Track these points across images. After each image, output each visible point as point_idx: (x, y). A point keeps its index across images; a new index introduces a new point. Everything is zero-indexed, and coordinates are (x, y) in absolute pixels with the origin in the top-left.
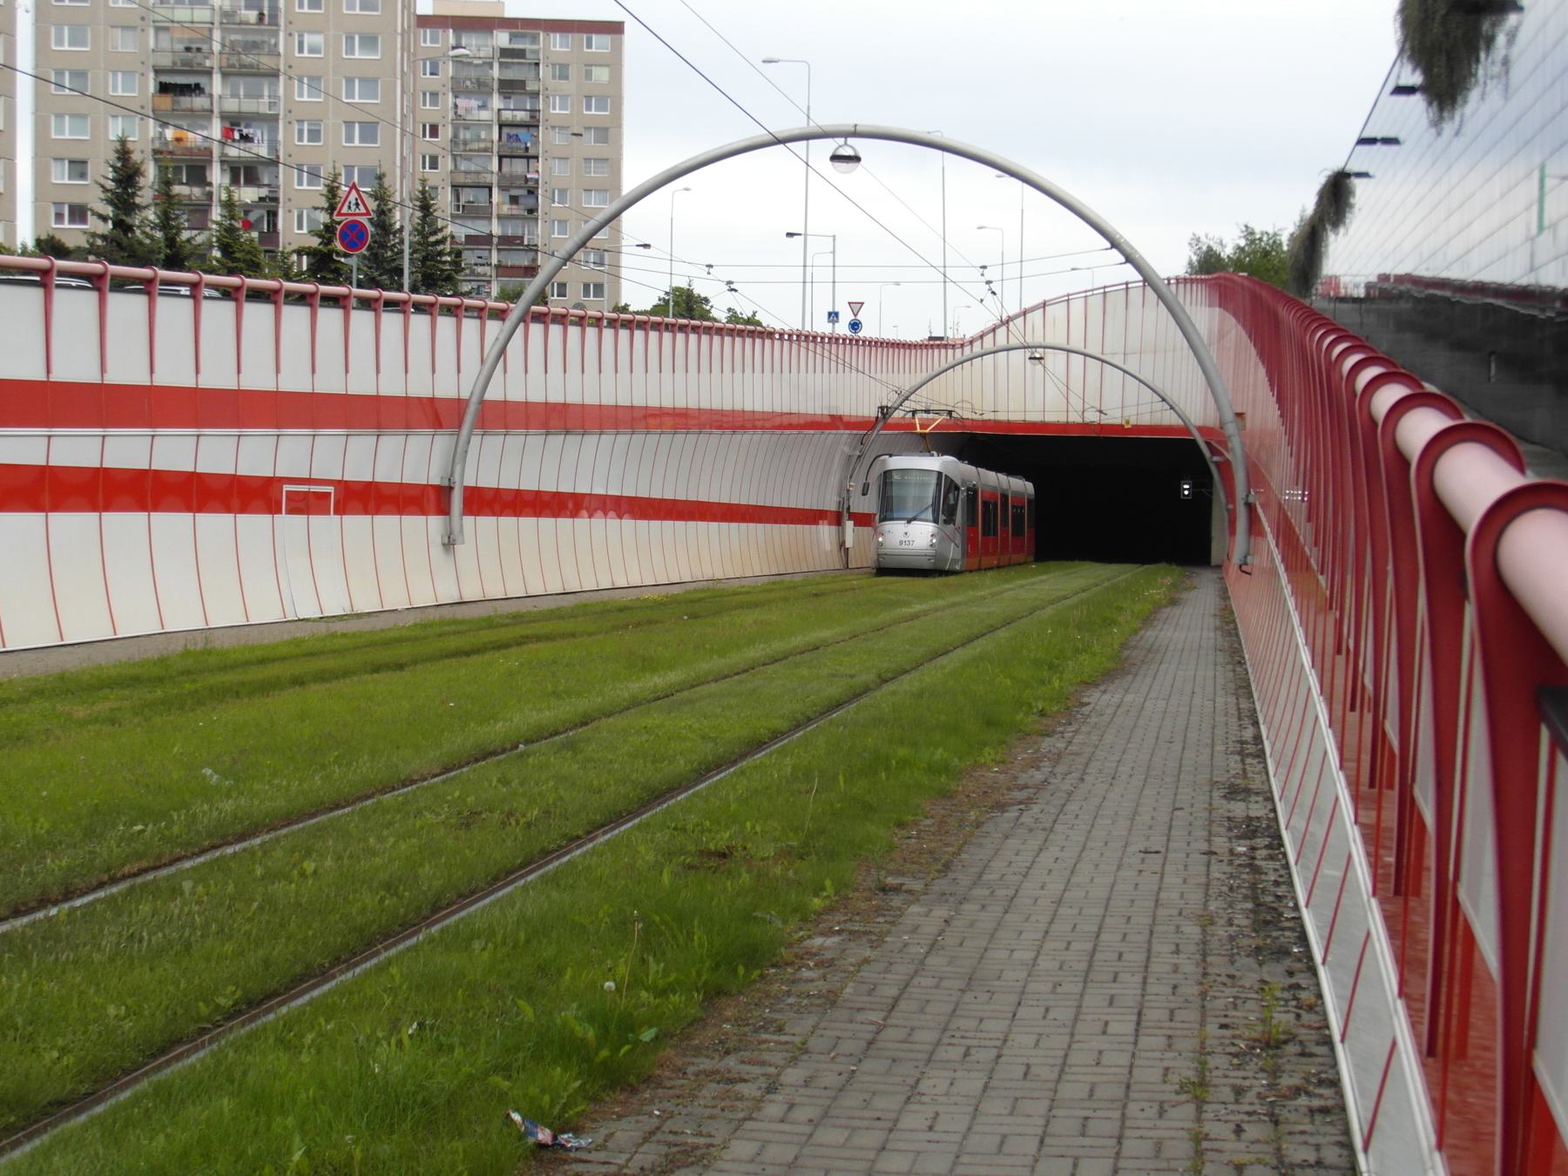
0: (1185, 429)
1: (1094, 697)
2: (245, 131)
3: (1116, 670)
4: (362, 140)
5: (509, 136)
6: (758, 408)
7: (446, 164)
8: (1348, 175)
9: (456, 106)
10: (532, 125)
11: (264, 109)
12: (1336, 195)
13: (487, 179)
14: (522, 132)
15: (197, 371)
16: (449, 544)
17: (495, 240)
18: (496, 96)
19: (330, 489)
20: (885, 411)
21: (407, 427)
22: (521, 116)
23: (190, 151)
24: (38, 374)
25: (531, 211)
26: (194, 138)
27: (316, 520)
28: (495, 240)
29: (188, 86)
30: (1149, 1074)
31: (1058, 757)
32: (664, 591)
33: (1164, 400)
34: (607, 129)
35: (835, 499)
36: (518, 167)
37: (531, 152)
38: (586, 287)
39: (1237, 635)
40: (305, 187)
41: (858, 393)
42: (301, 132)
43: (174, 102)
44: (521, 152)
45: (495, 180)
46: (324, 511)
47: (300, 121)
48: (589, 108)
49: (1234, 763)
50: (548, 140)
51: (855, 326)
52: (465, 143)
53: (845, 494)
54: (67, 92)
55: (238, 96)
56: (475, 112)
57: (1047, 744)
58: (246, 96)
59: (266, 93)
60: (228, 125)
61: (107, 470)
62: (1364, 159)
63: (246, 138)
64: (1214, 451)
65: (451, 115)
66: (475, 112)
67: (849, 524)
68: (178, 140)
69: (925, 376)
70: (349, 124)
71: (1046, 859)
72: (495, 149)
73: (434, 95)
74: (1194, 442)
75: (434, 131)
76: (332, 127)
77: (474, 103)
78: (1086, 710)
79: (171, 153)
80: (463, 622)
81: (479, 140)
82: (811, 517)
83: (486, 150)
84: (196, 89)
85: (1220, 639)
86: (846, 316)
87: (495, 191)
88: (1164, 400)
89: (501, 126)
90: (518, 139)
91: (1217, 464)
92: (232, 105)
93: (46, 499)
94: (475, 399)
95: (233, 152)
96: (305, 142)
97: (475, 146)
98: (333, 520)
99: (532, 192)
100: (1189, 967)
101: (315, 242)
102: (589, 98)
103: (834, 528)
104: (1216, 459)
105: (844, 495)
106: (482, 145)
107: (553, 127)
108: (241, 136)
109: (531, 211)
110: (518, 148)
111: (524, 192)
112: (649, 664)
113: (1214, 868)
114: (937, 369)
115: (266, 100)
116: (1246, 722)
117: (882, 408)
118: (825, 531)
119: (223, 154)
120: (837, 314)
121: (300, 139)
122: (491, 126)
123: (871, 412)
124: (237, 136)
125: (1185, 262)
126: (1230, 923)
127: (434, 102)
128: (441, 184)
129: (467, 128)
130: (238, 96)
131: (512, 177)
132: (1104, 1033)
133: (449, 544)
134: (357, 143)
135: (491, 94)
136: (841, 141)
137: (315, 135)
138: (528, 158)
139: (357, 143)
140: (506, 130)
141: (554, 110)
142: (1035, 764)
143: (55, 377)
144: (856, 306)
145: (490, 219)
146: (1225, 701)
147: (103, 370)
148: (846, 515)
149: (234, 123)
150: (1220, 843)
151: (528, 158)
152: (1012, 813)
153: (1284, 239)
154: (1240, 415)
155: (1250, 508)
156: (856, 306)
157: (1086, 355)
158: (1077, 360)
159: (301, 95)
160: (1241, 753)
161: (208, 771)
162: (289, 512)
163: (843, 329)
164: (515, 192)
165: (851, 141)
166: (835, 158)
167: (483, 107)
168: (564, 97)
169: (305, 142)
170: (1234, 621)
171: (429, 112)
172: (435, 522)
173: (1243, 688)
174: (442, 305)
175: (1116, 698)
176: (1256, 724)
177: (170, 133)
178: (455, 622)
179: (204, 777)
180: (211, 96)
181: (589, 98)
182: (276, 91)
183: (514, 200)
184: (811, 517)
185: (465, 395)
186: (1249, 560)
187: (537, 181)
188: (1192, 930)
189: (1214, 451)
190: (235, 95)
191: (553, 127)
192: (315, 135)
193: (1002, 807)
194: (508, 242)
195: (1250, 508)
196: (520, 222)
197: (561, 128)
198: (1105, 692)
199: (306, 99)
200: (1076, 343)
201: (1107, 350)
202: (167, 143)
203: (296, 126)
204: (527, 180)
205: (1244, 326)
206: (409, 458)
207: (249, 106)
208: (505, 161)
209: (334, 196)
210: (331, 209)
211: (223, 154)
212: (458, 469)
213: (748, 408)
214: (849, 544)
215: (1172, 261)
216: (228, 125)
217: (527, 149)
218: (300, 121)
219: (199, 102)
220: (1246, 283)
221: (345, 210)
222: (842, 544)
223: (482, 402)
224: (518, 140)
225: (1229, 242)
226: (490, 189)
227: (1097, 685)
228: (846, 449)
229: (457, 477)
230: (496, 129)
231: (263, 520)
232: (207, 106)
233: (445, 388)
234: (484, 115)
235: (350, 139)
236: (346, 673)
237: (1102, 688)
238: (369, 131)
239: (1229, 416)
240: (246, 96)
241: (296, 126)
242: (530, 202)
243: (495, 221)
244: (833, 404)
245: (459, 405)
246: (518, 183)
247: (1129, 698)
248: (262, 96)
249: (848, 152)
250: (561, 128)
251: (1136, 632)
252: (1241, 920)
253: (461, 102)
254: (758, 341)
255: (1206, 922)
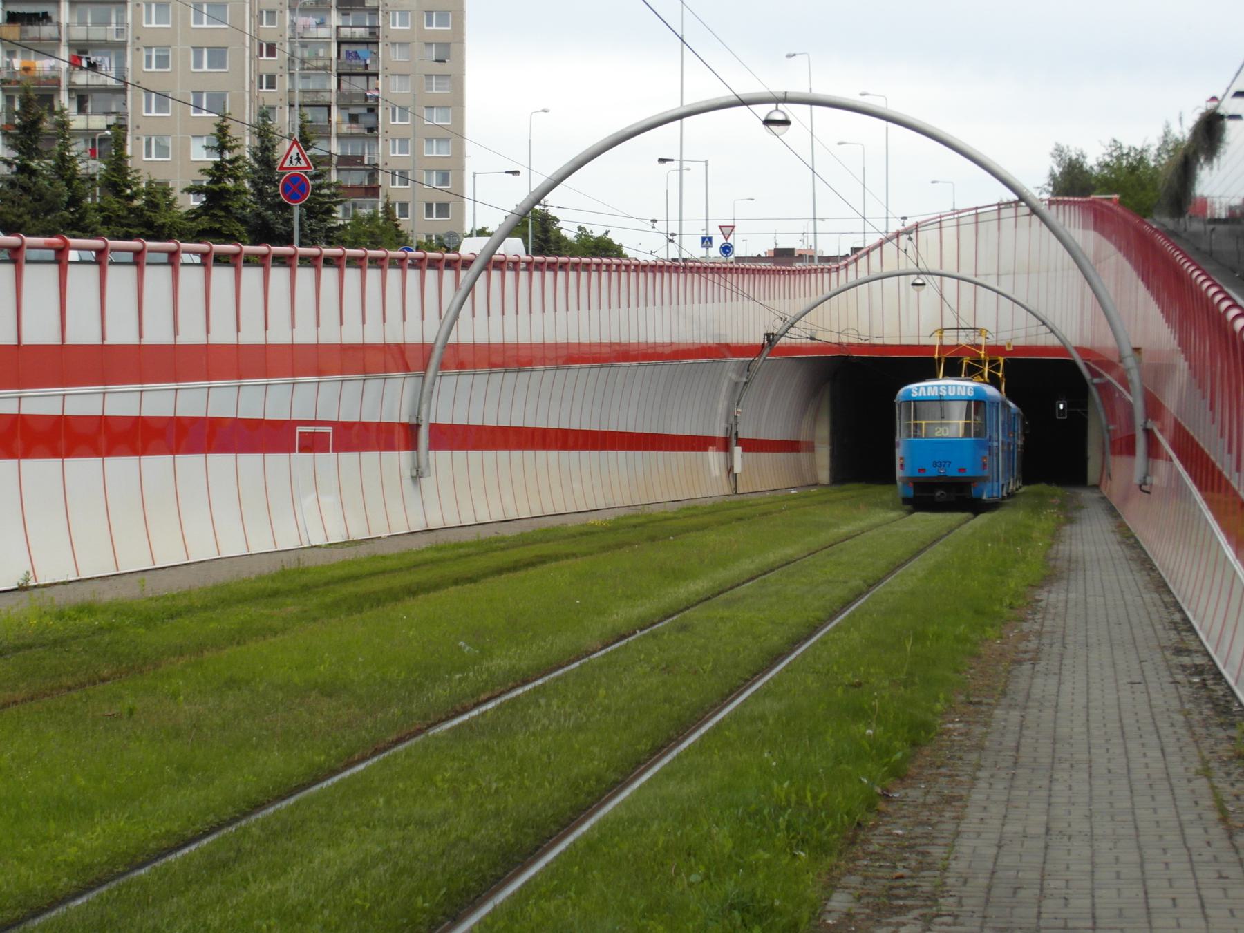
0: (1063, 350)
1: (1043, 595)
2: (93, 59)
3: (1051, 576)
4: (210, 66)
5: (347, 52)
6: (659, 340)
7: (283, 83)
8: (1222, 117)
9: (293, 24)
10: (372, 41)
11: (112, 37)
12: (1210, 130)
13: (326, 97)
14: (361, 49)
15: (238, 330)
16: (417, 476)
17: (335, 160)
18: (334, 13)
19: (329, 429)
20: (771, 338)
21: (364, 372)
22: (360, 33)
23: (38, 80)
24: (133, 340)
25: (371, 130)
26: (43, 65)
27: (320, 457)
28: (335, 160)
29: (36, 15)
30: (1176, 768)
31: (1039, 635)
32: (363, 551)
33: (1044, 323)
34: (448, 45)
35: (724, 425)
36: (359, 84)
37: (371, 69)
38: (429, 206)
39: (1141, 548)
40: (153, 114)
41: (743, 318)
42: (149, 58)
43: (22, 32)
44: (360, 70)
45: (334, 99)
46: (325, 450)
47: (149, 48)
48: (430, 23)
49: (1173, 634)
50: (388, 56)
51: (726, 249)
52: (303, 61)
53: (732, 420)
54: (205, 114)
55: (85, 24)
56: (313, 30)
57: (1025, 626)
58: (94, 24)
59: (114, 20)
60: (75, 53)
61: (179, 418)
62: (1230, 106)
63: (93, 66)
64: (1095, 374)
65: (288, 34)
66: (313, 30)
67: (737, 451)
68: (26, 69)
69: (814, 299)
70: (198, 50)
71: (1067, 687)
72: (334, 67)
73: (271, 13)
74: (1073, 364)
75: (271, 50)
76: (181, 54)
77: (312, 21)
78: (1043, 604)
79: (18, 82)
80: (468, 545)
81: (317, 58)
82: (699, 443)
83: (324, 68)
84: (44, 18)
85: (1128, 553)
86: (718, 241)
87: (334, 110)
88: (1044, 323)
89: (340, 43)
90: (357, 56)
91: (1096, 385)
92: (79, 33)
93: (18, 444)
94: (439, 344)
95: (82, 79)
96: (154, 69)
97: (314, 63)
98: (332, 456)
99: (372, 110)
100: (1182, 731)
101: (205, 180)
102: (429, 13)
103: (722, 454)
104: (1096, 380)
105: (732, 422)
106: (320, 63)
107: (394, 44)
108: (89, 63)
109: (371, 130)
110: (357, 65)
111: (364, 110)
112: (678, 575)
113: (1181, 689)
114: (827, 293)
115: (114, 27)
116: (1172, 609)
117: (768, 335)
118: (714, 457)
119: (71, 83)
120: (710, 239)
121: (149, 66)
122: (329, 44)
123: (759, 339)
124: (84, 64)
125: (1047, 173)
126: (1201, 713)
127: (271, 21)
128: (279, 104)
129: (304, 46)
130: (85, 24)
131: (352, 95)
132: (1067, 881)
133: (417, 476)
134: (205, 68)
135: (329, 11)
136: (773, 106)
137: (163, 61)
138: (368, 75)
139: (205, 68)
140: (344, 48)
141: (394, 26)
142: (1025, 637)
143: (145, 341)
144: (727, 230)
145: (329, 138)
146: (1150, 597)
147: (176, 332)
148: (734, 441)
149: (81, 53)
150: (1180, 677)
151: (368, 75)
152: (1027, 666)
153: (1153, 151)
154: (1137, 350)
155: (1149, 433)
156: (727, 230)
157: (959, 279)
158: (950, 284)
159: (149, 21)
160: (1176, 629)
161: (462, 643)
162: (302, 450)
163: (715, 252)
164: (354, 111)
165: (781, 106)
166: (768, 122)
167: (321, 24)
168: (404, 13)
169: (154, 69)
170: (1133, 536)
171: (269, 32)
172: (405, 456)
173: (1161, 586)
174: (392, 258)
175: (1062, 597)
176: (1181, 610)
177: (17, 63)
178: (459, 545)
179: (460, 648)
180: (59, 24)
181: (429, 13)
182: (123, 18)
183: (354, 119)
184: (699, 443)
185: (429, 339)
186: (1148, 480)
187: (377, 98)
188: (1179, 718)
189: (1095, 374)
190: (82, 23)
191: (394, 44)
192: (163, 61)
193: (1020, 662)
194: (348, 162)
195: (1149, 433)
196: (359, 142)
197: (401, 44)
198: (1050, 592)
199: (153, 25)
200: (950, 268)
201: (981, 271)
202: (14, 73)
203: (144, 53)
204: (366, 98)
205: (1127, 256)
206: (387, 400)
207: (97, 34)
208: (343, 78)
209: (225, 135)
210: (222, 148)
211: (71, 83)
212: (424, 408)
213: (651, 340)
214: (737, 469)
215: (1036, 177)
216: (75, 53)
217: (366, 66)
218: (149, 48)
219: (46, 31)
220: (1119, 210)
221: (287, 164)
222: (730, 470)
223: (446, 346)
224: (357, 60)
225: (1094, 156)
226: (329, 107)
227: (1041, 587)
228: (734, 377)
229: (423, 416)
230: (334, 47)
231: (283, 457)
232: (55, 35)
233: (412, 333)
234: (323, 33)
235: (198, 64)
236: (437, 586)
237: (1046, 589)
238: (218, 55)
239: (1127, 351)
240: (94, 24)
241: (144, 53)
242: (369, 120)
243: (334, 141)
244: (723, 332)
245: (425, 350)
246: (357, 101)
247: (1072, 596)
248: (109, 24)
249: (780, 117)
250: (401, 44)
251: (1051, 546)
252: (1206, 712)
253: (301, 20)
254: (658, 275)
255: (1187, 714)
